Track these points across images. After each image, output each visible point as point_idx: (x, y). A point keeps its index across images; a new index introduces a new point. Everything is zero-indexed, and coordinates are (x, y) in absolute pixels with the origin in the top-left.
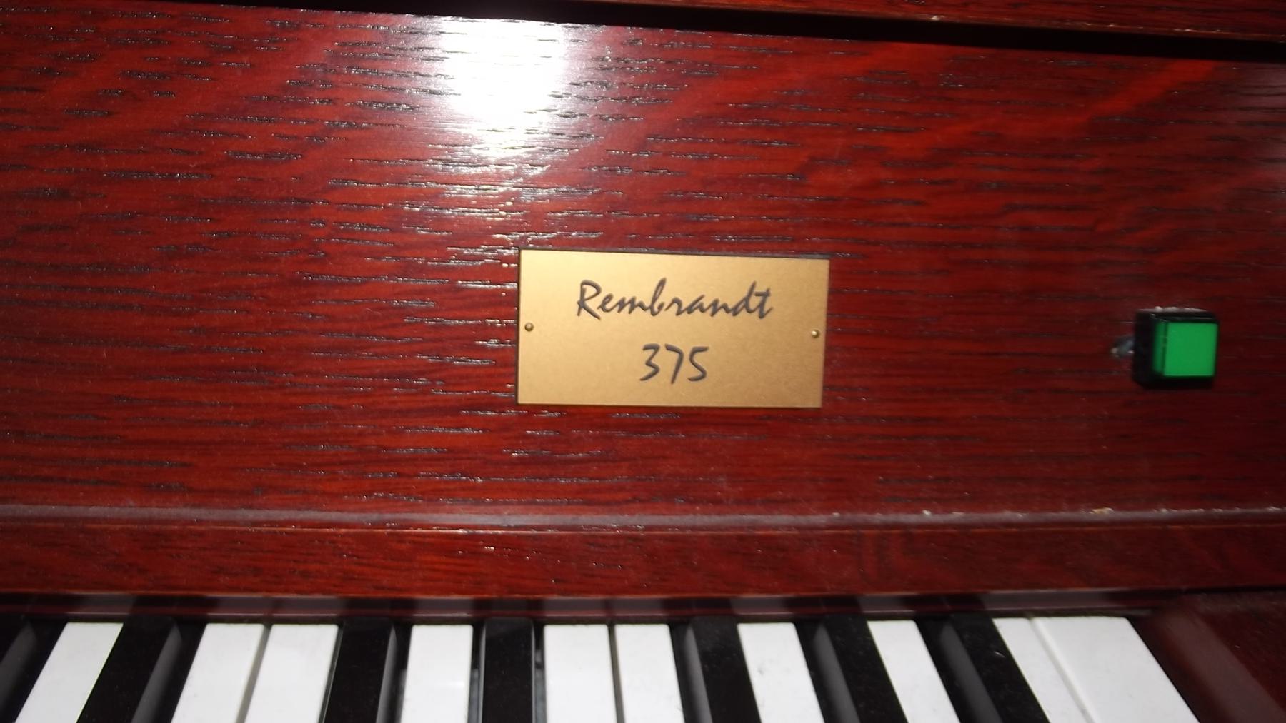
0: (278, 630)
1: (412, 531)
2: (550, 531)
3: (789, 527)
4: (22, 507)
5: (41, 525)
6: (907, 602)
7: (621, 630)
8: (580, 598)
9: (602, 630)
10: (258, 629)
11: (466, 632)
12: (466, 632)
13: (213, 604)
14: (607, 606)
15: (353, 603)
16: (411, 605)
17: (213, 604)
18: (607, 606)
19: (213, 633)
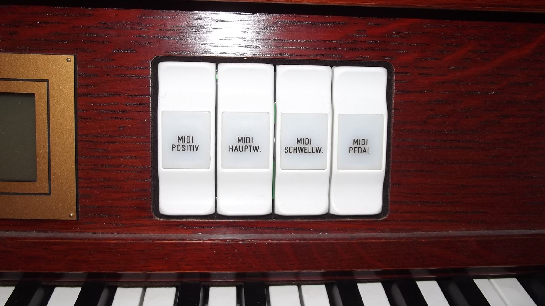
0: (149, 290)
1: (138, 241)
2: (217, 242)
3: (407, 238)
4: (274, 235)
5: (443, 240)
6: (378, 273)
7: (304, 288)
8: (223, 272)
9: (295, 288)
10: (140, 290)
11: (233, 291)
12: (233, 291)
13: (61, 276)
14: (296, 275)
15: (181, 276)
16: (208, 276)
17: (61, 276)
18: (296, 275)
19: (120, 292)
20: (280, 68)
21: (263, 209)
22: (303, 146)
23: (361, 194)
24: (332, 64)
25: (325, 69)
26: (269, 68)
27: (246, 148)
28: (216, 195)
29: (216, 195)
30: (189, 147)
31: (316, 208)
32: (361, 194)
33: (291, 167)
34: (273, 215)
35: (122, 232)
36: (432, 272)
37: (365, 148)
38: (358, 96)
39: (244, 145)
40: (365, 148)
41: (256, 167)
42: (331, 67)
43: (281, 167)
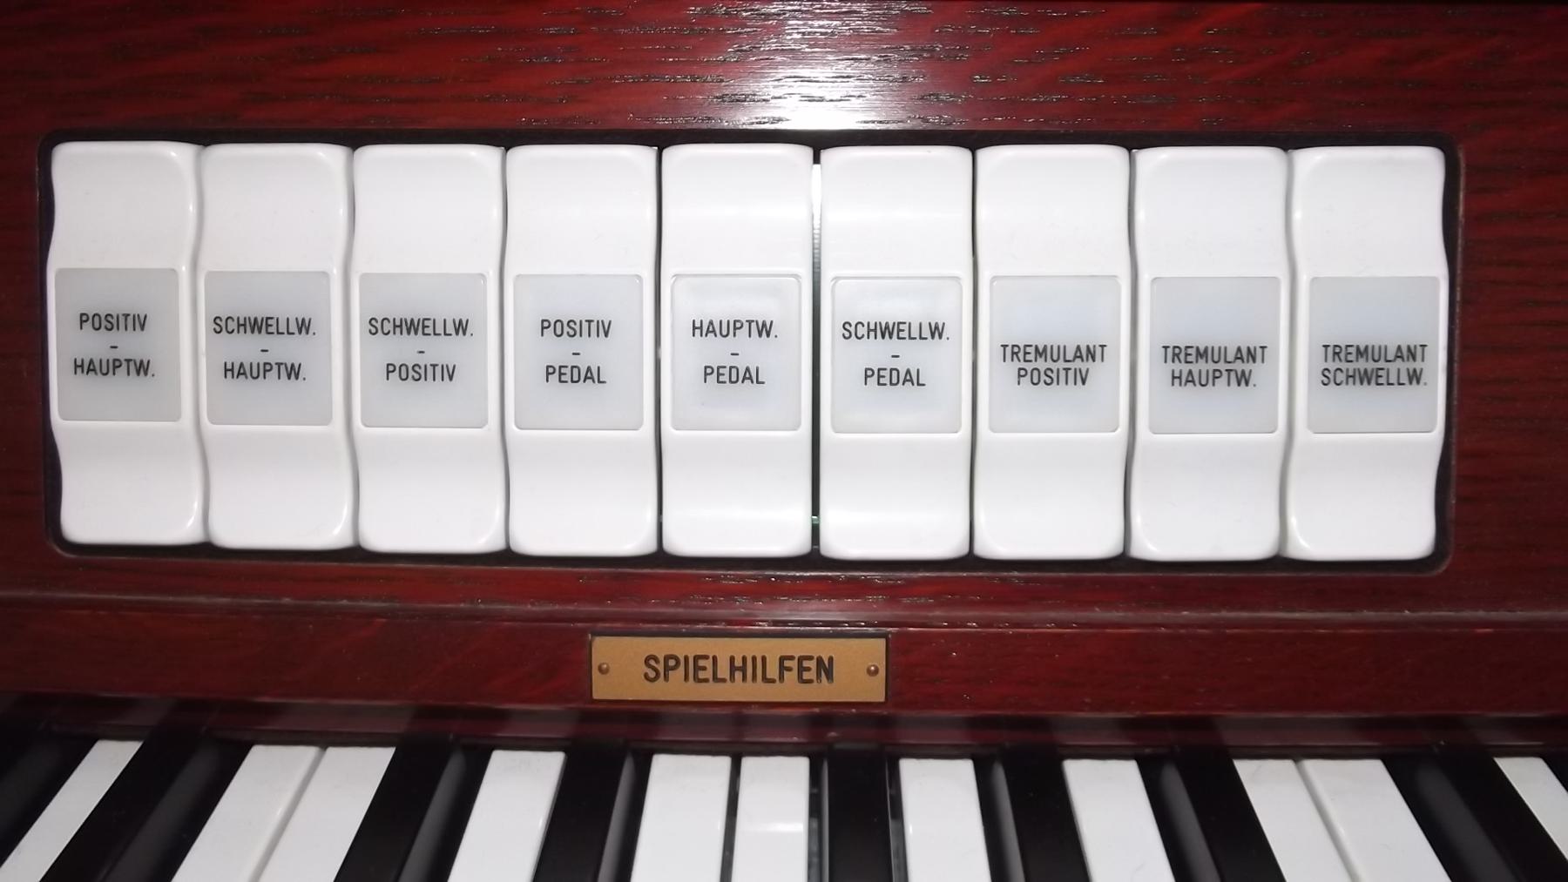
11: (801, 765)
12: (801, 765)
13: (271, 711)
17: (271, 711)
19: (500, 760)
20: (988, 156)
21: (1098, 543)
22: (1371, 365)
23: (1373, 499)
24: (1133, 140)
25: (1110, 157)
26: (956, 157)
27: (1216, 375)
28: (816, 510)
29: (816, 510)
30: (1063, 373)
31: (1247, 542)
32: (1373, 499)
33: (1026, 427)
34: (1279, 562)
35: (1293, 611)
36: (1364, 726)
37: (1190, 372)
38: (1365, 224)
39: (1211, 366)
40: (1190, 372)
41: (921, 430)
42: (1130, 150)
43: (1310, 427)
